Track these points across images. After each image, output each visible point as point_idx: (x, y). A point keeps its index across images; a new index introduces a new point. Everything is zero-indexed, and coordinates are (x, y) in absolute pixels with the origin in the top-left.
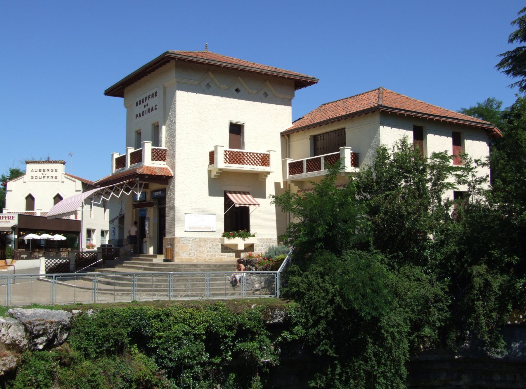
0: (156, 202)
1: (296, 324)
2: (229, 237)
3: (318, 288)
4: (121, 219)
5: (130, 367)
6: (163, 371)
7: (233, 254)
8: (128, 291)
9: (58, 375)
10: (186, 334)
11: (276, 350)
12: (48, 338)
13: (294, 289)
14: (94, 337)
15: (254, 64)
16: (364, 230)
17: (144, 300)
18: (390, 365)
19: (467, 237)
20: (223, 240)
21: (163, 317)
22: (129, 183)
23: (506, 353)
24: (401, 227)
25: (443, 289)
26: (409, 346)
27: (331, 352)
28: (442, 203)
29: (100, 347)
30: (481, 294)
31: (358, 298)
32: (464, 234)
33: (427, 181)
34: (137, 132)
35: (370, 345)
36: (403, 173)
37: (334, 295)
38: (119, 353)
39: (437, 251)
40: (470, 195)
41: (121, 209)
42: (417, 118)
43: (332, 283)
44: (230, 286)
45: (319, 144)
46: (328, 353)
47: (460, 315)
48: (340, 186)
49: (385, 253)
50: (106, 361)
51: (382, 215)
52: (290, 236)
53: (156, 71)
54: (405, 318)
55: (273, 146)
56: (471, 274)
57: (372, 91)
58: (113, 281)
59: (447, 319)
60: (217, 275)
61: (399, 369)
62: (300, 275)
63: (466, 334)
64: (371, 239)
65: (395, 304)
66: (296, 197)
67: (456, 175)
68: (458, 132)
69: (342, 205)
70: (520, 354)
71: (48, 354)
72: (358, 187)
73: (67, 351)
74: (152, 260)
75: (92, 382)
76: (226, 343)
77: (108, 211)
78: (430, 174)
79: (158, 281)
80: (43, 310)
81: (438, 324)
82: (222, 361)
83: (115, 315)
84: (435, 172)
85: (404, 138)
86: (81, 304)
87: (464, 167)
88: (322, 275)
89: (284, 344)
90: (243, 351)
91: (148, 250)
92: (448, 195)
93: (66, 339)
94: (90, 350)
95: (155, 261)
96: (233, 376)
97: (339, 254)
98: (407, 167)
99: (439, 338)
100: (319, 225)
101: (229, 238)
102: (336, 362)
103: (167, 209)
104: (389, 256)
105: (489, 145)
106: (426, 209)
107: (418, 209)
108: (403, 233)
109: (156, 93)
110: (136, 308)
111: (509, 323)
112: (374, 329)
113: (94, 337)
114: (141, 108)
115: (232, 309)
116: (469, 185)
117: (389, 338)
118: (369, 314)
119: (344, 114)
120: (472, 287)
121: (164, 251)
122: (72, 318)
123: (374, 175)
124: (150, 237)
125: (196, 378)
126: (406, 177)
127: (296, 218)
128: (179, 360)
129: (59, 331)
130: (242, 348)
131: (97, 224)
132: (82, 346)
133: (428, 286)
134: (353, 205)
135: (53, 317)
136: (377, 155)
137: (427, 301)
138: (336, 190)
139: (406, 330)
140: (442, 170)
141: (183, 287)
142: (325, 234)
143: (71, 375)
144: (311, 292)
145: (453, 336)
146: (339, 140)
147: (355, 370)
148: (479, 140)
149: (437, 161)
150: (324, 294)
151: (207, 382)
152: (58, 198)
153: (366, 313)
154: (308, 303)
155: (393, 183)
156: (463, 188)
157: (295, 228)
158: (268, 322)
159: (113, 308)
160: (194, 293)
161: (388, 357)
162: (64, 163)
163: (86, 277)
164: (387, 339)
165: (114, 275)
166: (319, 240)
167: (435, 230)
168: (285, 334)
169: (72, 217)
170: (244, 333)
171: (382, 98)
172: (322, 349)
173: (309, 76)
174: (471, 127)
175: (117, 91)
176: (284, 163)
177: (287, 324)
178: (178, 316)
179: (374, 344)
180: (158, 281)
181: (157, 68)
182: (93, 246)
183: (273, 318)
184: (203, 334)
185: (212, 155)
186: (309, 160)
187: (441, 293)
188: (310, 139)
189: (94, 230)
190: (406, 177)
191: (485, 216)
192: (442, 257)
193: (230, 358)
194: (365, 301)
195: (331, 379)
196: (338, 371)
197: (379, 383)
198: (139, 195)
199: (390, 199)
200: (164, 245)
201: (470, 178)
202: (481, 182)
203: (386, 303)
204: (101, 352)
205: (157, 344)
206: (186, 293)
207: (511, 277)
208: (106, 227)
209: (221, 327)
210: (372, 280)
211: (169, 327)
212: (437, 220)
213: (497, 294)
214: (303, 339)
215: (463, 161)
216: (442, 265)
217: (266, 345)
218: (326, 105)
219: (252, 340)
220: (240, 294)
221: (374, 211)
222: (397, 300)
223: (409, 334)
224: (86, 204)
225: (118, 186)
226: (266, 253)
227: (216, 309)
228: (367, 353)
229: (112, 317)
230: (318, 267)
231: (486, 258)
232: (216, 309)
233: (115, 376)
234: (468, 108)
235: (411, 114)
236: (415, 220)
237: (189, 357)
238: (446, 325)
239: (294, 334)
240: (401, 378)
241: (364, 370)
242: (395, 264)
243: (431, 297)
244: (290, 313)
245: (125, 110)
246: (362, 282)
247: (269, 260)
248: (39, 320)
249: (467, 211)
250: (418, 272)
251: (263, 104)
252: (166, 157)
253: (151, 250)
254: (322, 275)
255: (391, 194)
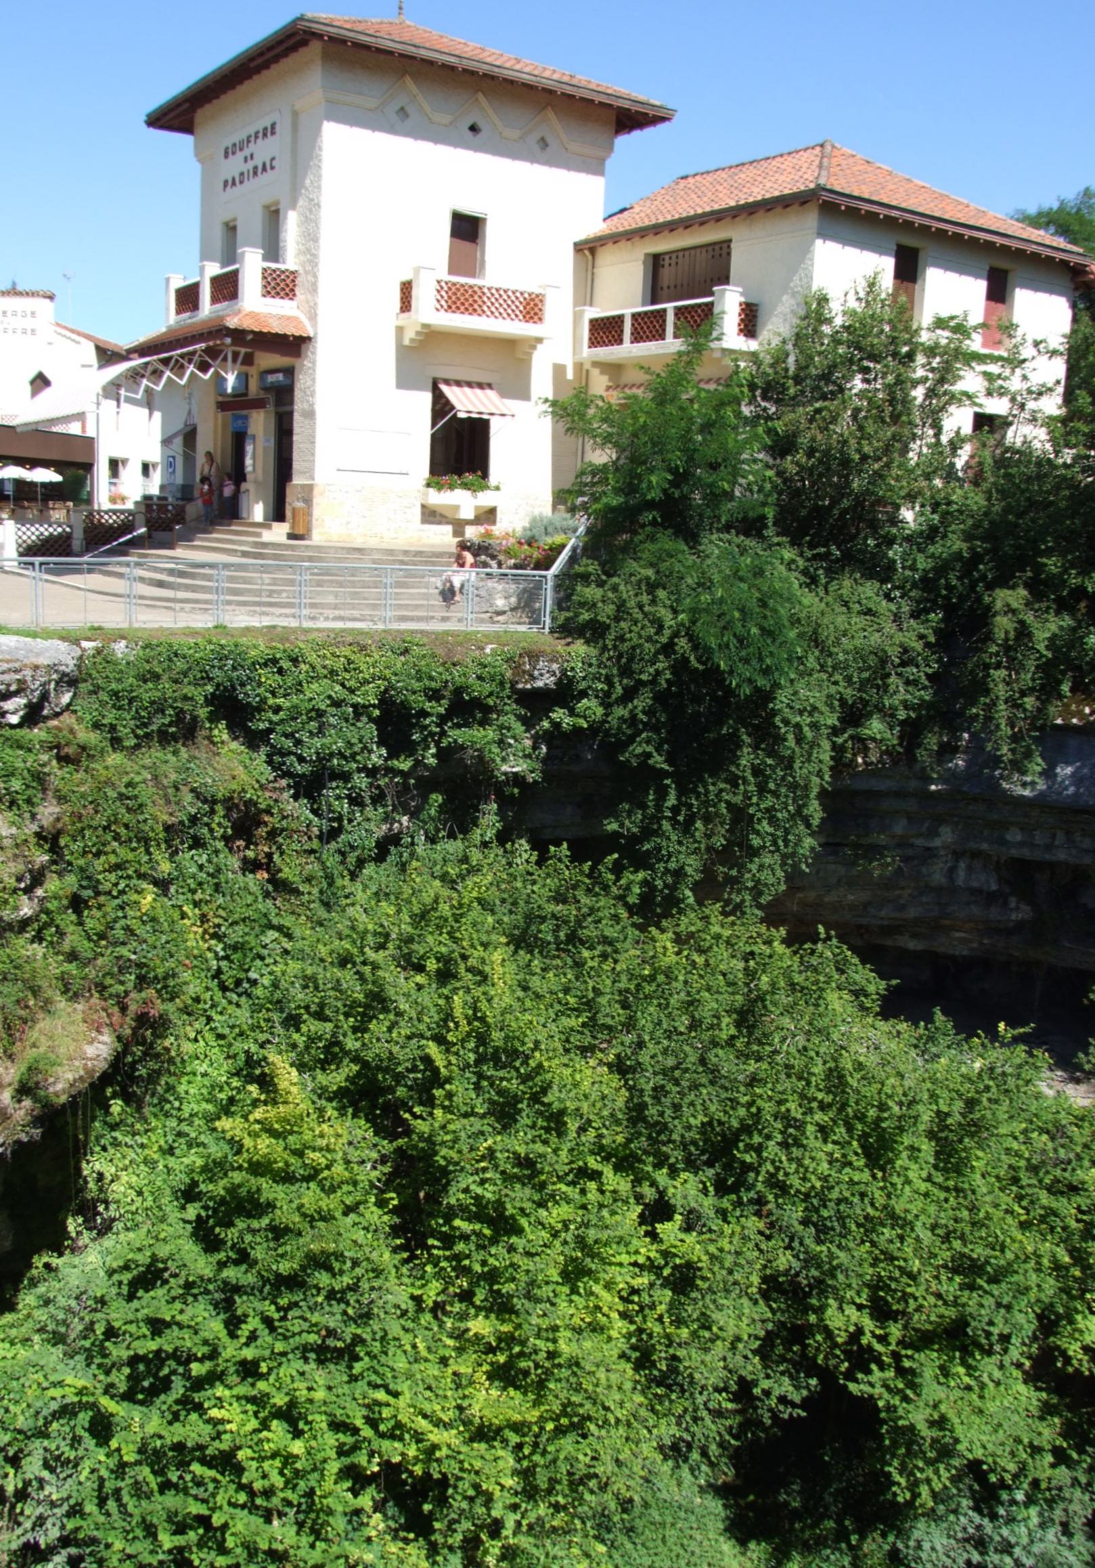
0: (271, 398)
1: (583, 694)
2: (440, 487)
3: (640, 616)
4: (190, 436)
5: (210, 771)
6: (284, 782)
7: (449, 529)
8: (206, 602)
9: (54, 782)
10: (337, 704)
11: (535, 747)
12: (30, 701)
13: (586, 616)
14: (131, 701)
15: (518, 61)
16: (755, 488)
17: (243, 625)
18: (787, 796)
19: (991, 523)
20: (426, 495)
21: (286, 664)
22: (208, 351)
23: (1042, 785)
24: (843, 489)
25: (921, 637)
26: (832, 758)
27: (659, 759)
28: (944, 439)
29: (145, 725)
30: (1006, 654)
31: (727, 646)
32: (986, 514)
33: (915, 383)
34: (227, 224)
35: (745, 750)
36: (861, 359)
37: (676, 635)
38: (186, 738)
39: (919, 550)
40: (1011, 424)
41: (189, 413)
42: (908, 225)
43: (671, 607)
44: (438, 602)
45: (666, 275)
46: (651, 762)
47: (954, 695)
48: (708, 381)
49: (799, 545)
50: (159, 754)
51: (800, 457)
52: (581, 493)
53: (274, 66)
54: (829, 696)
55: (555, 278)
56: (988, 608)
57: (806, 150)
58: (171, 579)
59: (923, 703)
60: (409, 574)
61: (805, 805)
62: (601, 584)
63: (960, 739)
64: (770, 512)
65: (811, 662)
66: (601, 404)
67: (985, 374)
68: (1006, 268)
69: (707, 428)
70: (1072, 790)
71: (30, 736)
72: (752, 387)
73: (72, 731)
74: (259, 535)
75: (128, 798)
76: (425, 727)
77: (157, 415)
78: (923, 366)
79: (274, 582)
80: (15, 638)
81: (902, 715)
82: (414, 767)
83: (176, 655)
84: (936, 362)
85: (876, 274)
86: (100, 628)
87: (1005, 355)
88: (652, 587)
89: (555, 736)
90: (462, 748)
91: (250, 511)
92: (959, 420)
93: (69, 705)
94: (123, 731)
95: (267, 536)
96: (437, 798)
97: (692, 538)
98: (872, 346)
99: (900, 745)
100: (651, 471)
101: (439, 490)
102: (668, 782)
103: (296, 416)
104: (809, 554)
105: (1074, 306)
106: (905, 450)
107: (887, 449)
108: (845, 503)
109: (273, 126)
110: (223, 642)
111: (1059, 721)
112: (758, 714)
113: (131, 701)
114: (235, 165)
115: (440, 651)
116: (1013, 400)
117: (791, 737)
118: (750, 681)
119: (733, 203)
120: (989, 638)
121: (288, 513)
122: (81, 658)
123: (791, 359)
124: (255, 482)
125: (356, 801)
126: (866, 370)
127: (598, 452)
128: (319, 759)
129: (52, 685)
130: (460, 741)
131: (133, 450)
132: (105, 721)
133: (889, 627)
134: (735, 428)
135: (38, 655)
136: (802, 313)
137: (884, 660)
138: (700, 390)
139: (829, 722)
140: (952, 359)
141: (330, 599)
142: (665, 491)
143: (82, 782)
144: (623, 624)
145: (932, 741)
146: (714, 267)
147: (707, 801)
148: (1051, 291)
149: (943, 336)
150: (652, 631)
151: (381, 810)
152: (40, 382)
153: (742, 679)
154: (615, 647)
155: (834, 383)
156: (997, 406)
157: (594, 475)
158: (520, 686)
159: (173, 640)
160: (356, 613)
161: (783, 778)
162: (51, 298)
163: (110, 568)
164: (785, 740)
165: (172, 566)
166: (651, 505)
167: (919, 500)
168: (559, 714)
169: (74, 429)
170: (466, 708)
171: (828, 168)
172: (639, 750)
173: (653, 101)
174: (1035, 257)
175: (177, 116)
176: (577, 317)
177: (565, 692)
178: (318, 662)
179: (756, 747)
180: (274, 582)
181: (276, 59)
182: (123, 499)
183: (534, 678)
184: (374, 706)
185: (406, 289)
186: (639, 314)
187: (918, 646)
188: (644, 263)
189: (125, 462)
190: (866, 370)
191: (1040, 477)
192: (930, 564)
193: (432, 761)
194: (743, 653)
195: (653, 816)
196: (671, 800)
197: (758, 833)
198: (231, 380)
199: (824, 419)
200: (288, 499)
201: (1015, 384)
202: (1040, 394)
203: (790, 660)
204: (147, 735)
205: (271, 722)
206: (337, 613)
207: (1079, 622)
208: (155, 454)
209: (414, 693)
210: (763, 603)
211: (299, 687)
212: (928, 477)
213: (1042, 656)
214: (595, 729)
215: (1006, 341)
216: (927, 583)
217: (513, 737)
218: (691, 180)
219: (483, 723)
220: (460, 620)
221: (782, 446)
222: (817, 653)
223: (835, 731)
224: (106, 397)
225: (182, 356)
226: (525, 529)
227: (406, 651)
228: (738, 766)
229: (170, 660)
230: (643, 567)
231: (1029, 574)
232: (406, 651)
233: (177, 789)
234: (1032, 210)
235: (894, 213)
236: (878, 475)
237: (341, 755)
238: (919, 717)
239: (578, 716)
240: (808, 826)
241: (727, 802)
242: (821, 572)
243: (893, 652)
244: (573, 669)
245: (196, 167)
246: (742, 610)
247: (530, 545)
248: (8, 661)
249: (1000, 463)
250: (870, 593)
251: (536, 166)
252: (297, 290)
253: (258, 512)
254: (652, 587)
255: (826, 408)
